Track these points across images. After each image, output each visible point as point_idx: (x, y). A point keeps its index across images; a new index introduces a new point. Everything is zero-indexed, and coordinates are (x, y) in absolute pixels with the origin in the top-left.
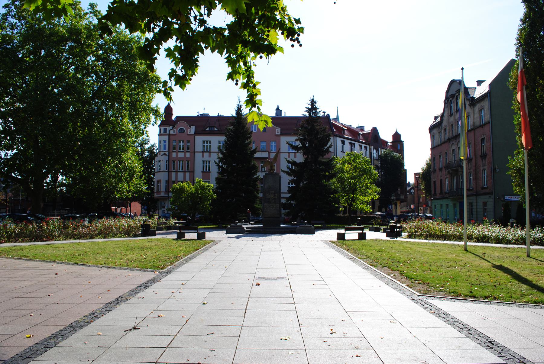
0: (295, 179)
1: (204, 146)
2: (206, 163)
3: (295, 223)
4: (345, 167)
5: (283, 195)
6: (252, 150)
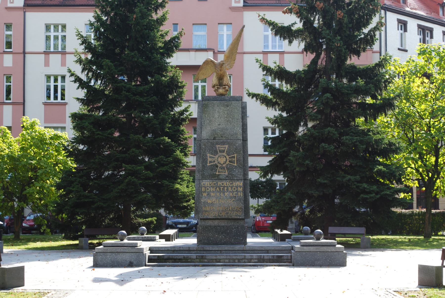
0: (284, 114)
1: (48, 38)
2: (56, 80)
3: (285, 232)
4: (416, 85)
5: (252, 162)
6: (167, 38)
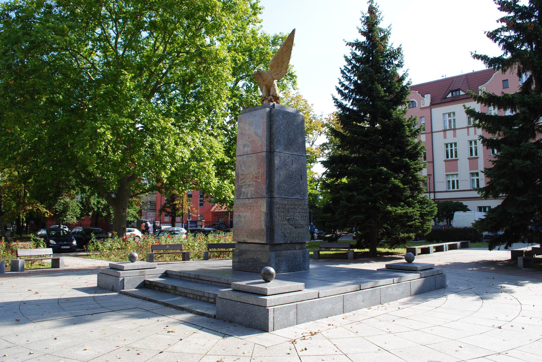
2: (451, 147)
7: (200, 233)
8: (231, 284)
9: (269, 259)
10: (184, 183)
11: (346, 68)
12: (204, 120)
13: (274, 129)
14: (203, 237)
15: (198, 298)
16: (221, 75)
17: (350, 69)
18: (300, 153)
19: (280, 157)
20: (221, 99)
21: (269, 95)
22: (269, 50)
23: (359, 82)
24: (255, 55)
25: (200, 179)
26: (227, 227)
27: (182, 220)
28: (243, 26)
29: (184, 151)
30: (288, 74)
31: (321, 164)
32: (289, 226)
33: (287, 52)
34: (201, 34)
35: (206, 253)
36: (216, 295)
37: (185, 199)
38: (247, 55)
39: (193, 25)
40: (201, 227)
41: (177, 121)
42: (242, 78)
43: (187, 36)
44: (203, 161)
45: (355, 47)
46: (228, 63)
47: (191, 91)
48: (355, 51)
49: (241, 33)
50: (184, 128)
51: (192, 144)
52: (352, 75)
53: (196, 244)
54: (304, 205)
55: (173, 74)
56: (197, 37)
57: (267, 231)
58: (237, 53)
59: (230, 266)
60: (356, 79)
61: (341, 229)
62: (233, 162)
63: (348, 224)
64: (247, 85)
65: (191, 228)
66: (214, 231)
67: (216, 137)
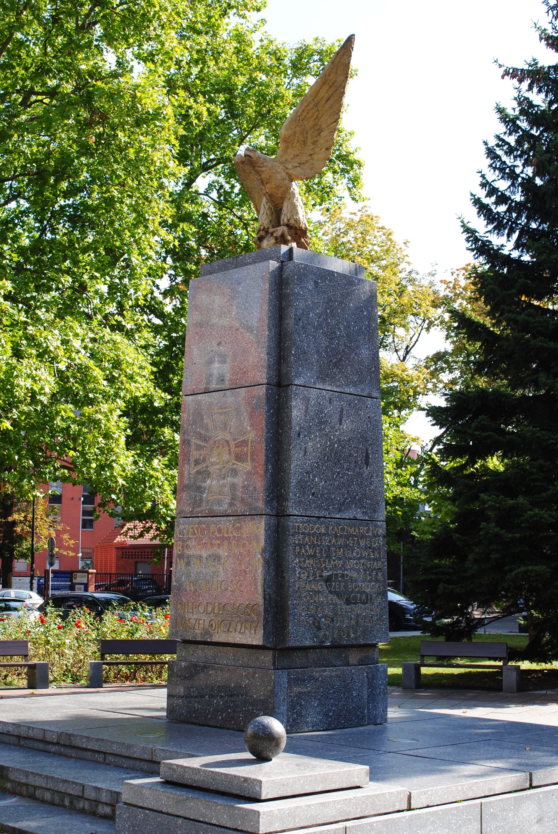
7: (80, 607)
8: (159, 763)
9: (272, 691)
10: (37, 464)
11: (502, 142)
12: (98, 287)
13: (290, 322)
14: (90, 619)
15: (67, 803)
16: (146, 159)
17: (513, 144)
18: (363, 390)
19: (306, 400)
20: (146, 227)
21: (278, 224)
22: (282, 89)
23: (538, 181)
24: (243, 101)
25: (83, 454)
26: (159, 592)
27: (32, 569)
28: (210, 17)
29: (39, 373)
30: (339, 157)
31: (428, 415)
32: (331, 596)
33: (330, 102)
34: (91, 42)
35: (97, 668)
36: (118, 794)
37: (40, 510)
38: (222, 103)
39: (69, 14)
40: (86, 590)
41: (21, 287)
42: (205, 168)
43: (53, 46)
44: (91, 402)
45: (527, 82)
46: (166, 125)
47: (62, 203)
48: (527, 95)
49: (203, 40)
50: (40, 308)
51: (61, 353)
52: (519, 163)
53: (67, 641)
54: (374, 536)
55: (11, 152)
56: (80, 48)
57: (265, 610)
58: (192, 95)
59: (162, 709)
60: (531, 175)
61: (484, 604)
62: (178, 406)
63: (503, 590)
64: (221, 187)
65: (57, 593)
66: (122, 602)
67: (129, 334)
